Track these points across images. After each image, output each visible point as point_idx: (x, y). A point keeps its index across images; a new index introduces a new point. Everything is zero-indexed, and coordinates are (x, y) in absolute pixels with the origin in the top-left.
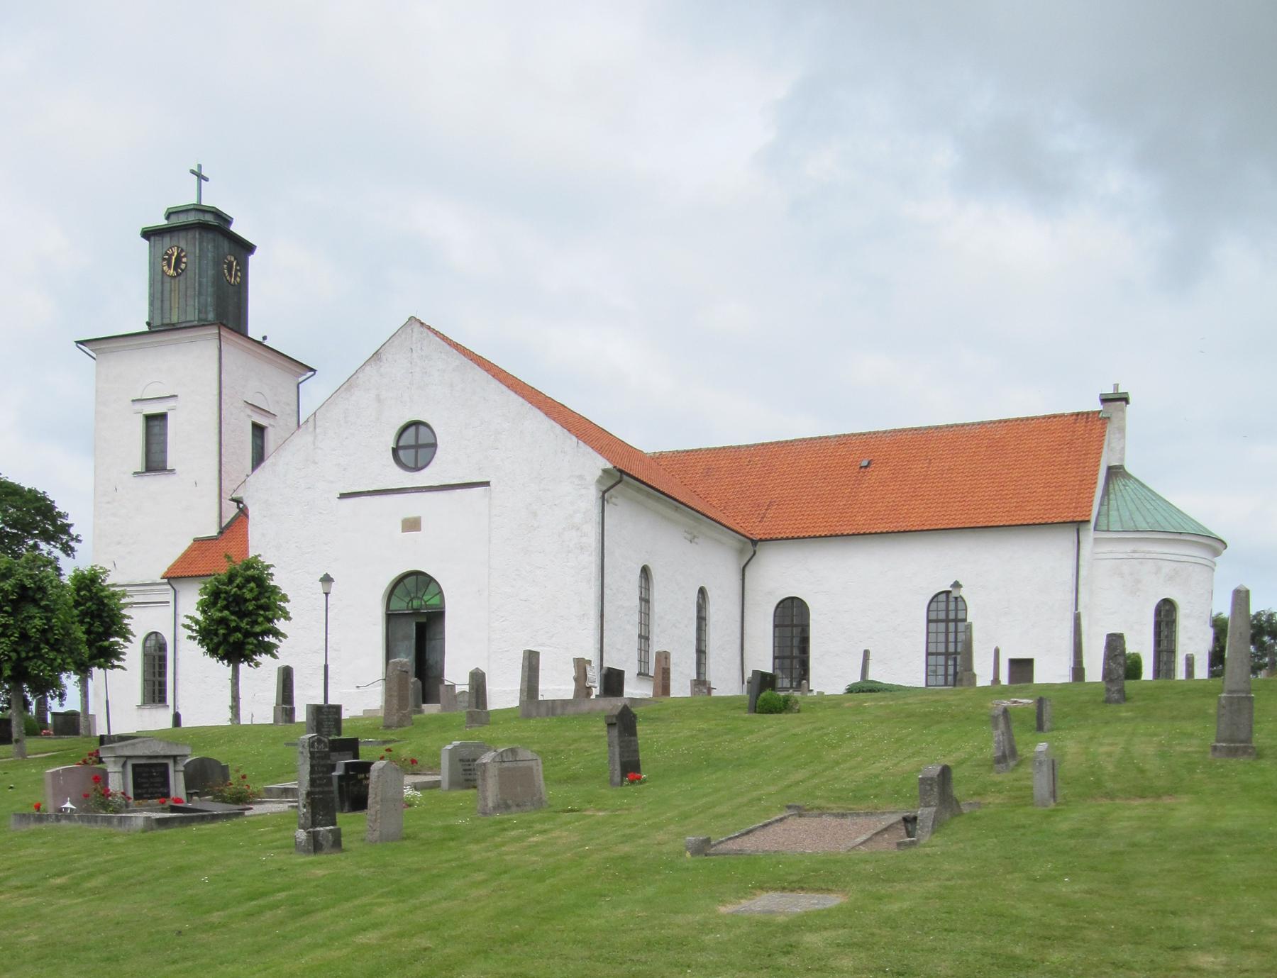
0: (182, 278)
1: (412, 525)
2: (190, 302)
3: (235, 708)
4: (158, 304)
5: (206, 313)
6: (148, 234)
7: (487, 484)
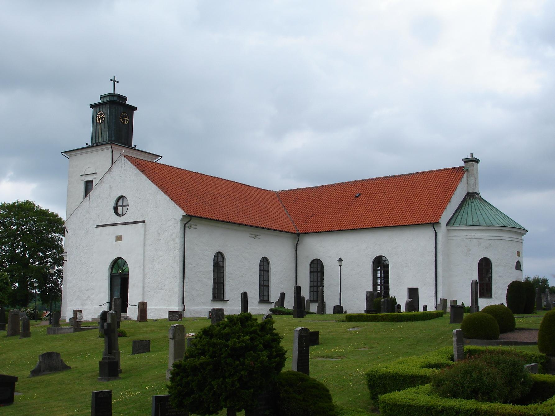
0: (103, 124)
1: (119, 238)
2: (105, 133)
3: (537, 330)
4: (94, 135)
5: (112, 137)
6: (92, 106)
7: (144, 222)
